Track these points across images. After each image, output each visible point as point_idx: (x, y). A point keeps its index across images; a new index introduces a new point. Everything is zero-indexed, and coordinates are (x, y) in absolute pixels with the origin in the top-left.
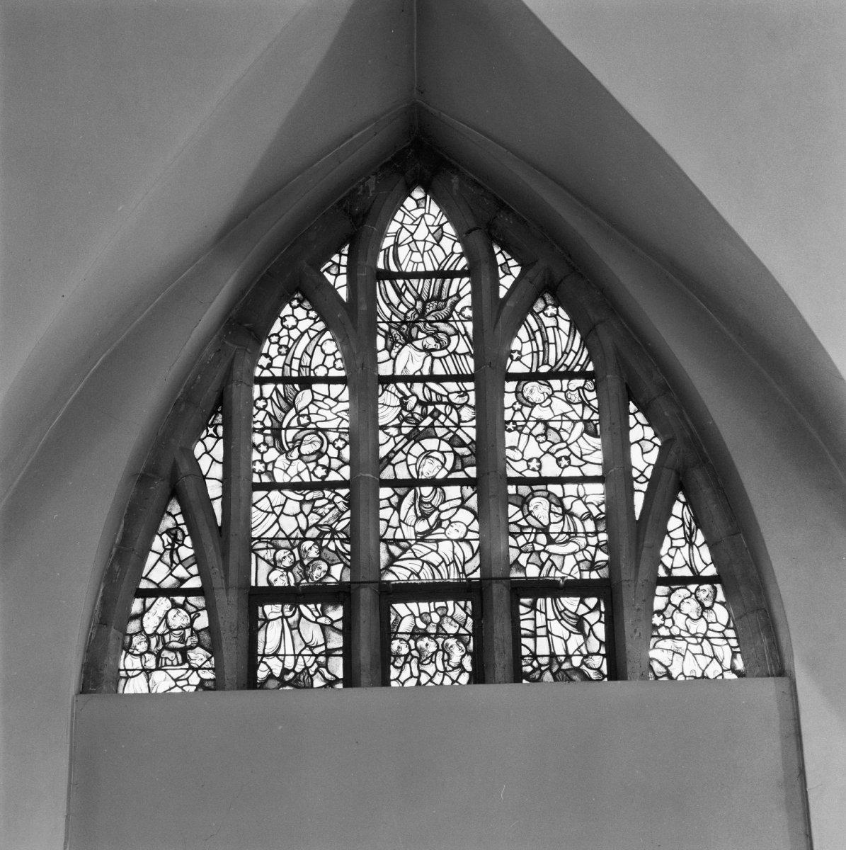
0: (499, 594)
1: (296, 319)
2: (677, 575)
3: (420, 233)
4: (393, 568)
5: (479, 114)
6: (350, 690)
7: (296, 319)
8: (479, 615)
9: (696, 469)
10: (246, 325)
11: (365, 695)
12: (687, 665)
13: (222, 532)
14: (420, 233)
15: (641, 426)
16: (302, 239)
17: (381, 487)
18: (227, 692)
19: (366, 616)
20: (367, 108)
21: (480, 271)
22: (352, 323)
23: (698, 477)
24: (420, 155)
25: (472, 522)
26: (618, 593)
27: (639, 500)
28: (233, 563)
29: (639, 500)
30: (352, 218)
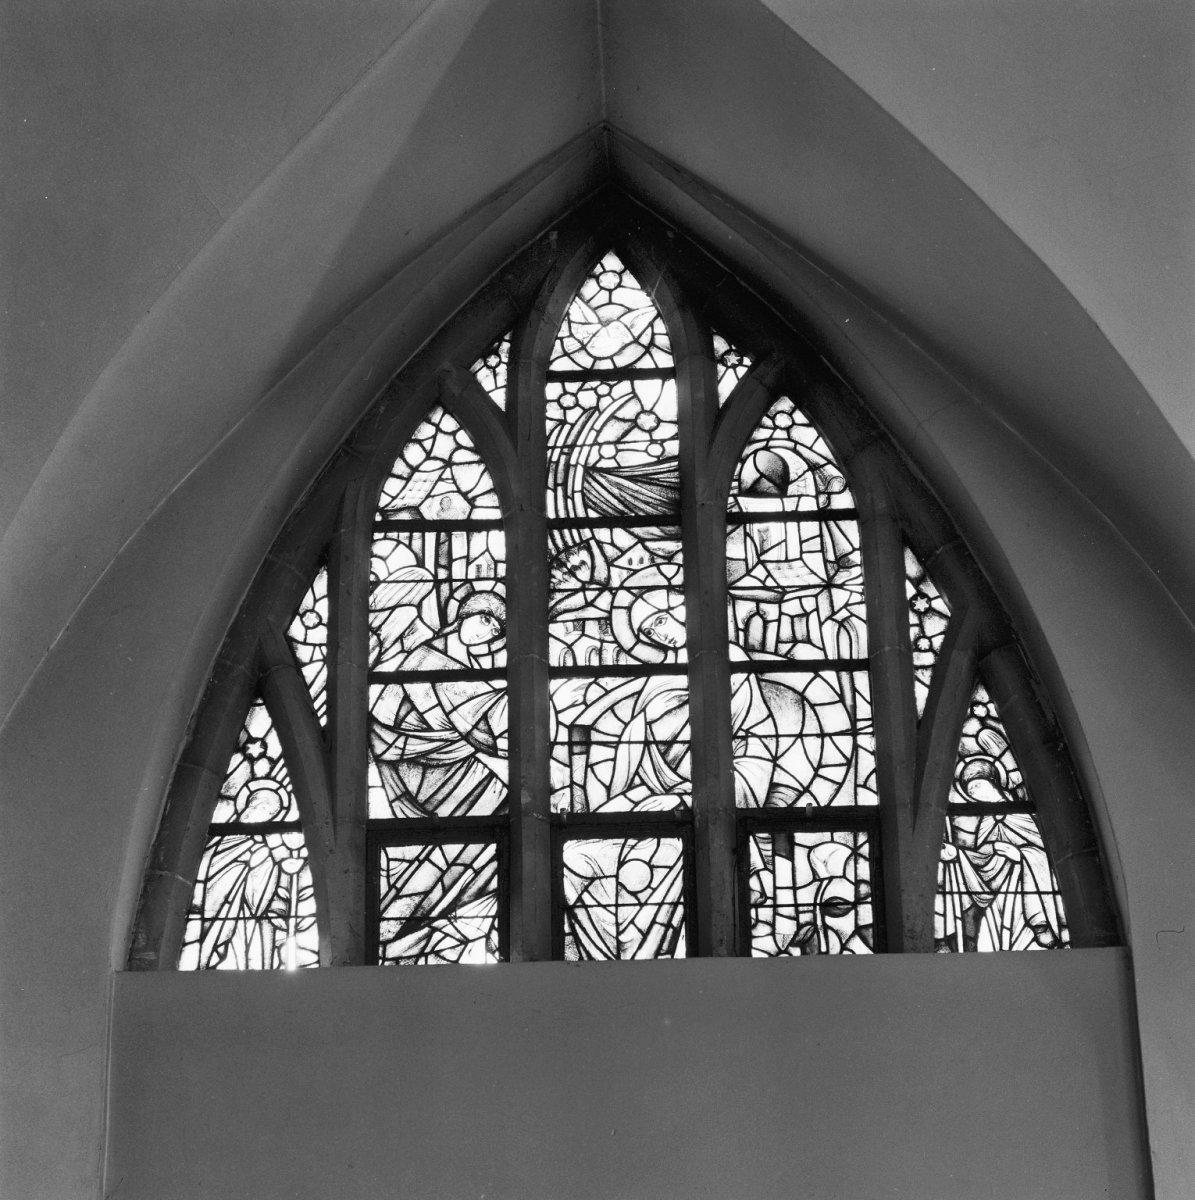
0: (531, 834)
1: (442, 435)
2: (866, 804)
3: (613, 314)
4: (422, 798)
5: (712, 144)
6: (697, 960)
7: (442, 435)
8: (506, 864)
9: (997, 645)
10: (367, 446)
11: (720, 966)
12: (247, 952)
13: (326, 737)
14: (613, 314)
15: (416, 614)
16: (452, 324)
17: (686, 664)
18: (906, 955)
19: (531, 860)
20: (524, 139)
21: (692, 366)
22: (513, 446)
23: (999, 662)
24: (611, 207)
25: (764, 720)
26: (896, 830)
27: (921, 694)
28: (342, 776)
29: (921, 694)
30: (516, 298)
